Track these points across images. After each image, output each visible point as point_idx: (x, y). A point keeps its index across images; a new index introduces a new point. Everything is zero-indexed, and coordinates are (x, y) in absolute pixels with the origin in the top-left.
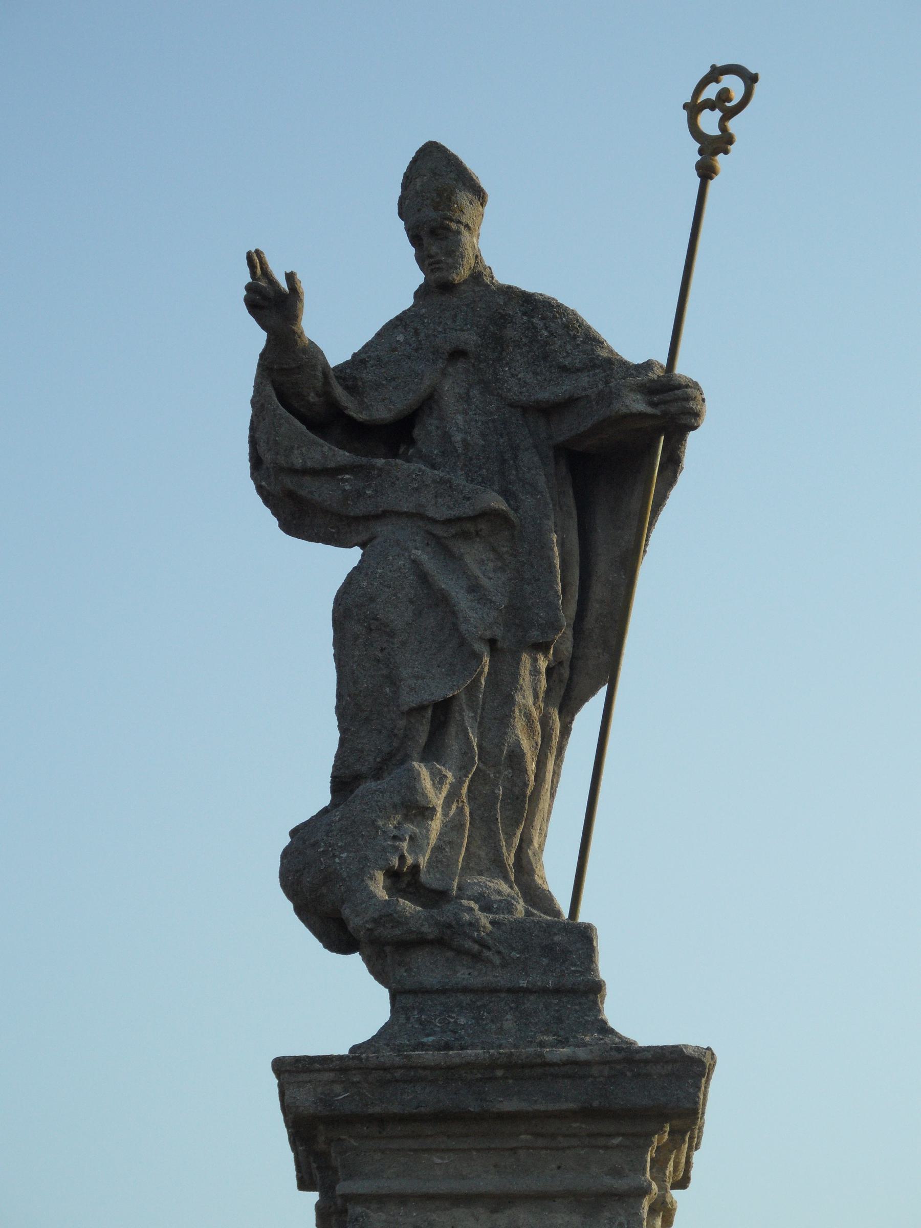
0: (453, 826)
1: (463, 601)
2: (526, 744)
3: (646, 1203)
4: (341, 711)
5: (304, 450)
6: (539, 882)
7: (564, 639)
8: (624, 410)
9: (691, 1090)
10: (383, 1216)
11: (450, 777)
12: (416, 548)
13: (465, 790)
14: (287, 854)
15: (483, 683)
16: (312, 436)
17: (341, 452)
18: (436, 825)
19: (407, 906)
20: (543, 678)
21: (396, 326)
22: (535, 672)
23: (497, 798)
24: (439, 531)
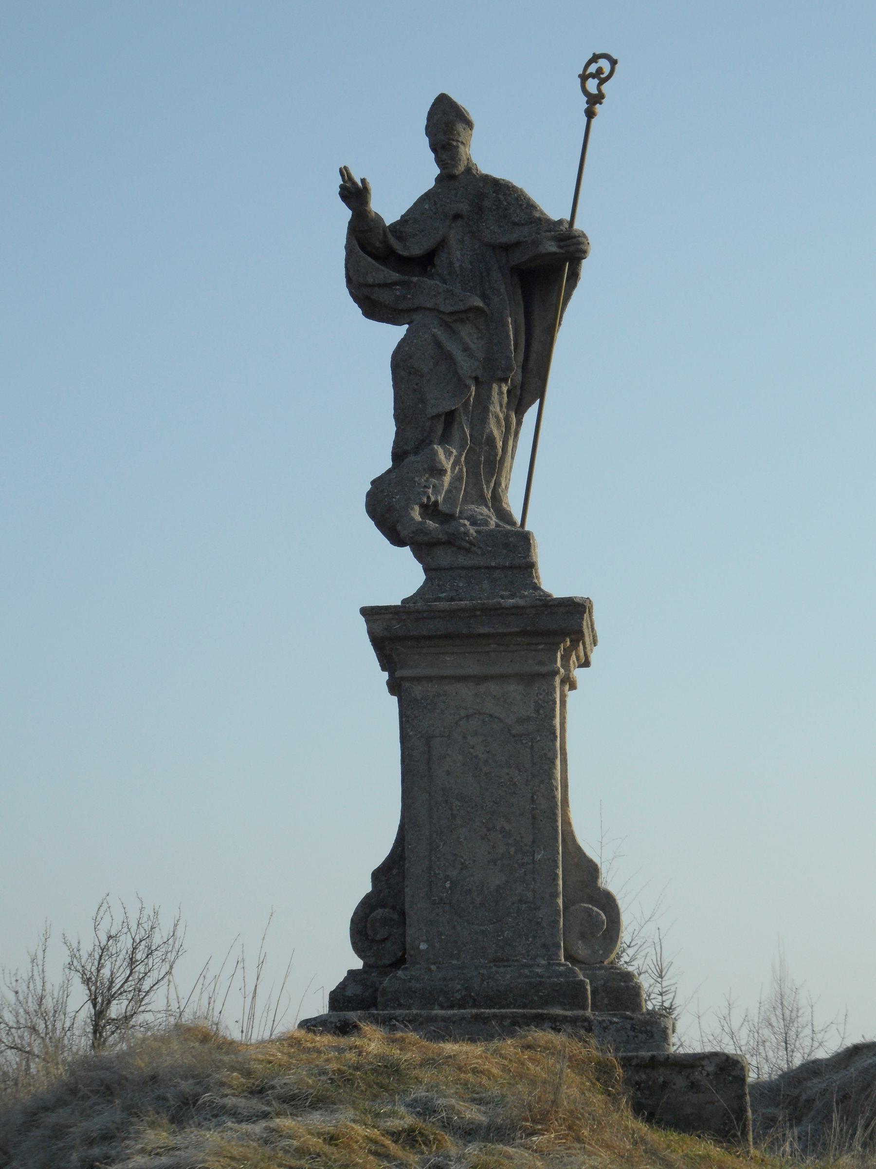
0: (457, 479)
1: (459, 356)
2: (496, 433)
3: (558, 680)
4: (397, 417)
5: (374, 273)
6: (505, 506)
7: (516, 374)
8: (544, 251)
9: (579, 621)
10: (420, 688)
11: (455, 452)
12: (435, 328)
13: (463, 459)
14: (369, 495)
15: (472, 401)
16: (377, 265)
17: (394, 274)
18: (447, 479)
19: (431, 524)
20: (505, 396)
21: (424, 200)
22: (500, 393)
23: (481, 462)
24: (447, 319)
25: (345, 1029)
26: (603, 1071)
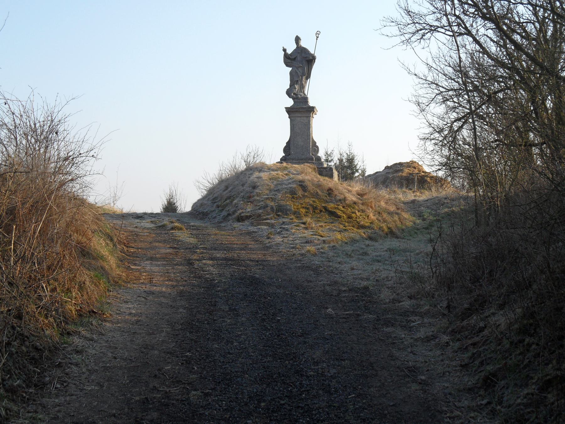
0: (298, 89)
1: (298, 72)
7: (307, 75)
25: (282, 163)
26: (315, 169)
